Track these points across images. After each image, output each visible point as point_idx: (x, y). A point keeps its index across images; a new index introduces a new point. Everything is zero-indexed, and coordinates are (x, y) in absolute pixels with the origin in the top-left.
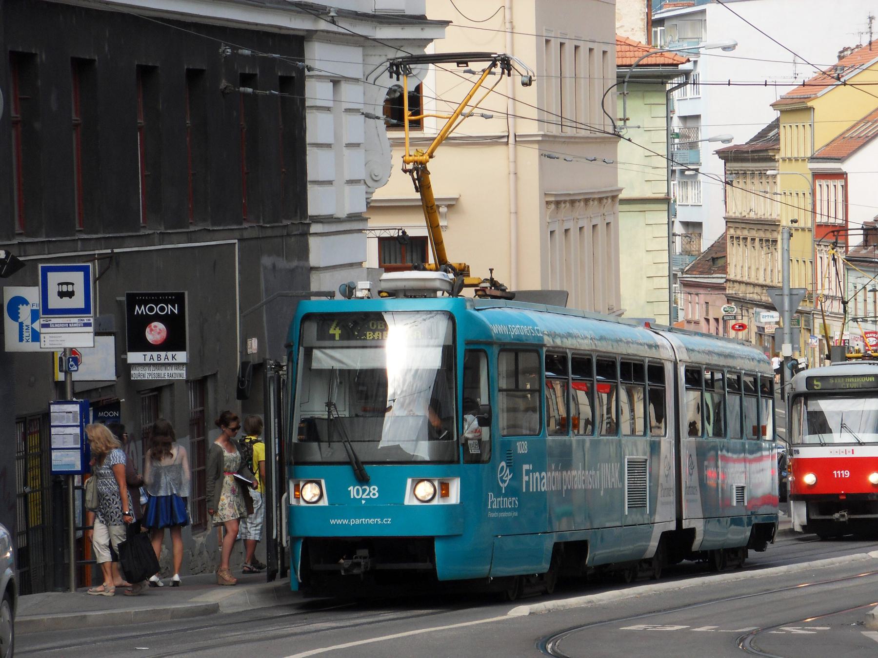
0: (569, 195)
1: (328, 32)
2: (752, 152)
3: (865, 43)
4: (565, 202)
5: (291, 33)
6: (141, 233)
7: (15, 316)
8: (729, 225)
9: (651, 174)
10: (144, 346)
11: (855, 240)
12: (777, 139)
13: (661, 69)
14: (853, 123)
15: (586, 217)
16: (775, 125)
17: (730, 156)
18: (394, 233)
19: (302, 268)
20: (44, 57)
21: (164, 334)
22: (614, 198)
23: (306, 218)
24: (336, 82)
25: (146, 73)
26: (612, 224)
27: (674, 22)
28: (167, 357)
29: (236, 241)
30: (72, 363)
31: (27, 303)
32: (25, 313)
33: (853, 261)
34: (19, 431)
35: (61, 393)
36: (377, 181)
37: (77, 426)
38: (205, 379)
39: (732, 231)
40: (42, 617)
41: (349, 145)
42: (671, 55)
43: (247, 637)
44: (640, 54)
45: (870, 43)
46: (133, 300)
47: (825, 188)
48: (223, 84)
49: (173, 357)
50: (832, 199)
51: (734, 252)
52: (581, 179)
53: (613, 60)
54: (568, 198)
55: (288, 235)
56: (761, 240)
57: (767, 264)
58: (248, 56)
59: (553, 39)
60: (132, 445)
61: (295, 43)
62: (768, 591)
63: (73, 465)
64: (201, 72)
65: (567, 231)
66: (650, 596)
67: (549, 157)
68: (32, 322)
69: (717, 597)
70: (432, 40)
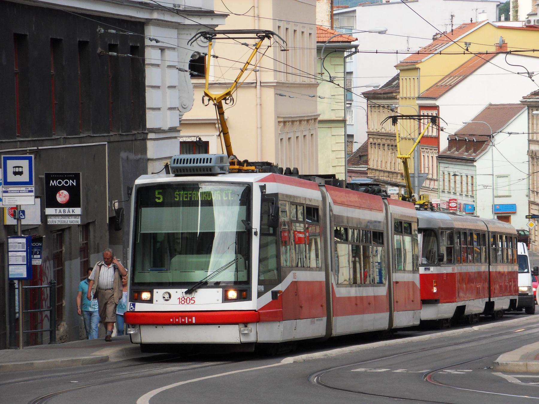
1: (158, 20)
2: (384, 94)
3: (449, 30)
4: (289, 121)
5: (138, 20)
6: (53, 138)
8: (370, 136)
9: (335, 107)
10: (54, 204)
11: (444, 144)
12: (398, 86)
13: (341, 44)
14: (443, 77)
15: (300, 130)
16: (397, 78)
17: (369, 96)
18: (194, 139)
19: (143, 159)
21: (67, 197)
22: (315, 119)
23: (145, 130)
24: (162, 49)
25: (55, 42)
26: (314, 135)
29: (106, 143)
30: (21, 214)
33: (441, 158)
35: (12, 231)
37: (24, 251)
38: (88, 224)
39: (371, 140)
40: (8, 364)
41: (170, 87)
45: (452, 30)
46: (49, 177)
48: (99, 50)
52: (297, 107)
54: (290, 120)
55: (136, 140)
56: (388, 145)
57: (392, 160)
58: (114, 33)
60: (48, 262)
61: (139, 26)
62: (424, 350)
63: (22, 274)
65: (289, 138)
66: (358, 352)
67: (280, 95)
69: (397, 352)
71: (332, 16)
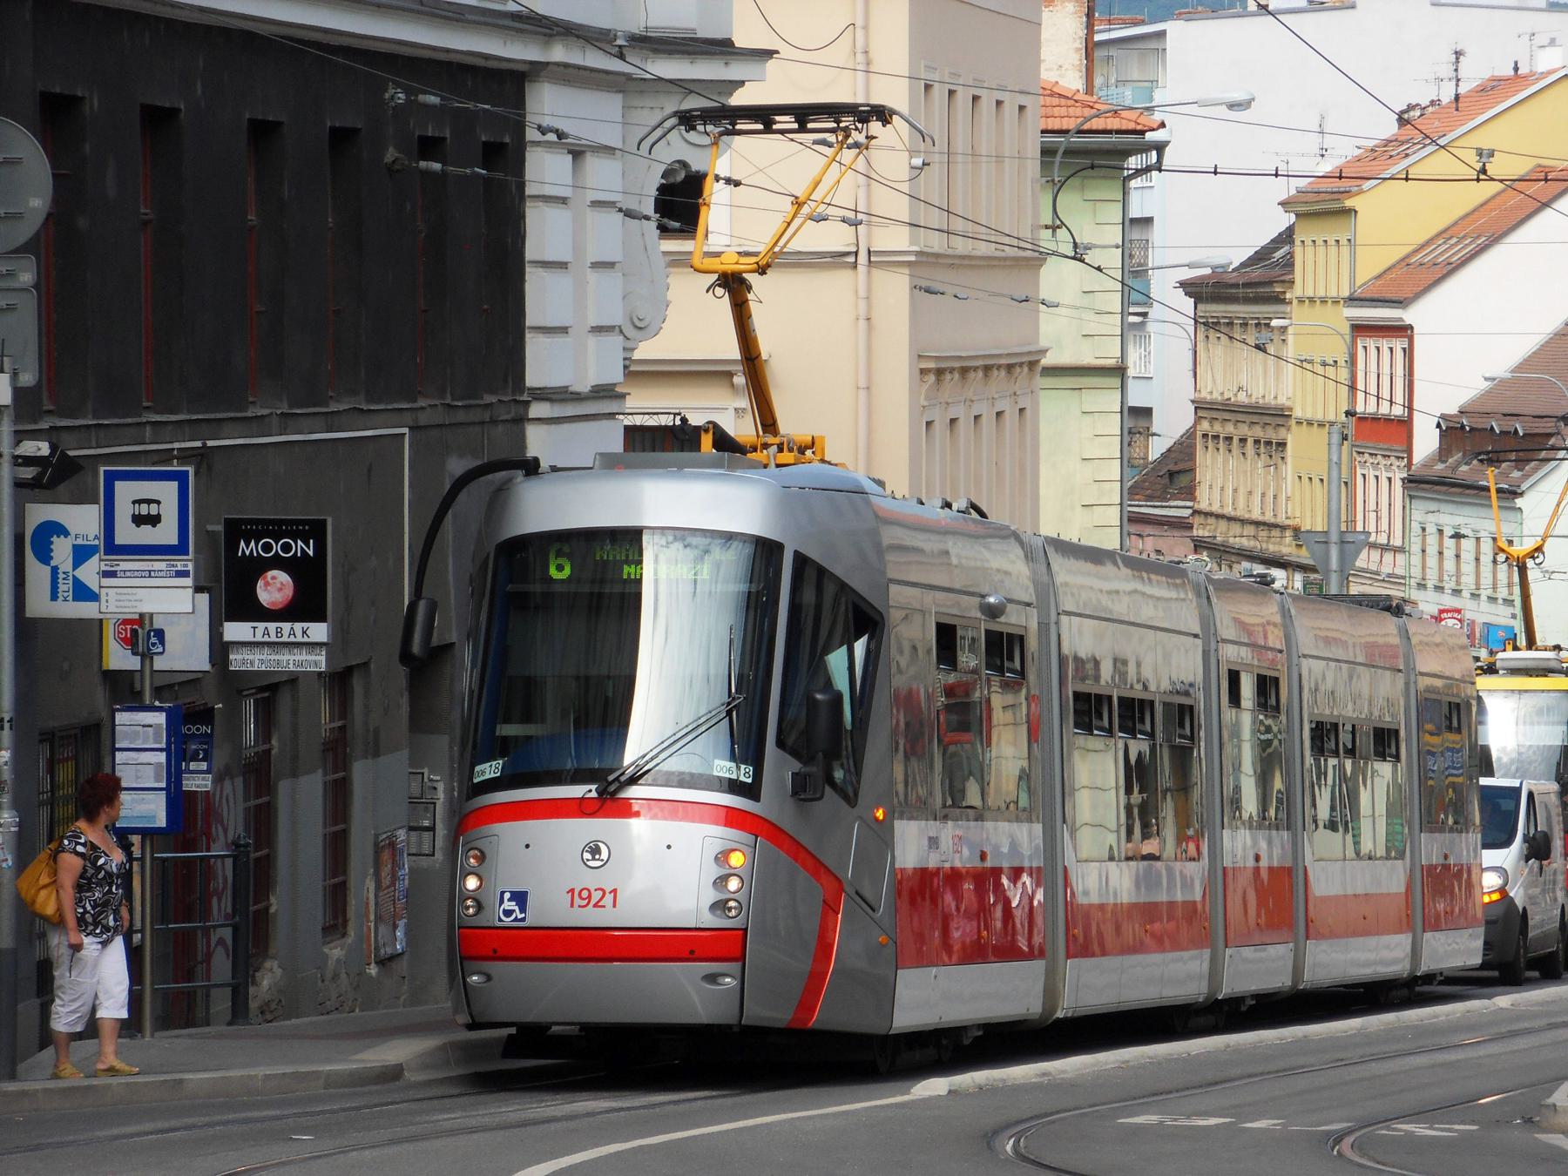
0: (960, 358)
1: (566, 65)
2: (1246, 285)
3: (1447, 96)
4: (952, 370)
5: (504, 66)
6: (249, 414)
7: (44, 555)
10: (251, 610)
11: (1426, 441)
12: (1289, 263)
13: (1114, 138)
15: (988, 396)
16: (1287, 237)
18: (666, 421)
20: (96, 102)
21: (289, 592)
22: (1032, 365)
24: (577, 154)
25: (262, 132)
26: (1028, 412)
27: (1113, 52)
28: (292, 633)
29: (406, 430)
30: (153, 640)
31: (66, 533)
32: (62, 550)
33: (1417, 484)
34: (45, 750)
35: (124, 690)
36: (642, 328)
38: (348, 671)
39: (1205, 425)
41: (596, 265)
42: (1133, 115)
43: (474, 1122)
44: (1088, 112)
45: (1457, 98)
46: (237, 530)
47: (1373, 352)
48: (391, 154)
49: (304, 633)
50: (1386, 370)
51: (1209, 462)
52: (978, 330)
53: (1036, 122)
54: (957, 365)
55: (494, 422)
56: (1257, 442)
57: (1266, 485)
58: (435, 106)
59: (936, 85)
61: (510, 84)
64: (355, 131)
65: (953, 421)
67: (928, 291)
68: (75, 566)
70: (742, 83)
71: (1090, 48)
